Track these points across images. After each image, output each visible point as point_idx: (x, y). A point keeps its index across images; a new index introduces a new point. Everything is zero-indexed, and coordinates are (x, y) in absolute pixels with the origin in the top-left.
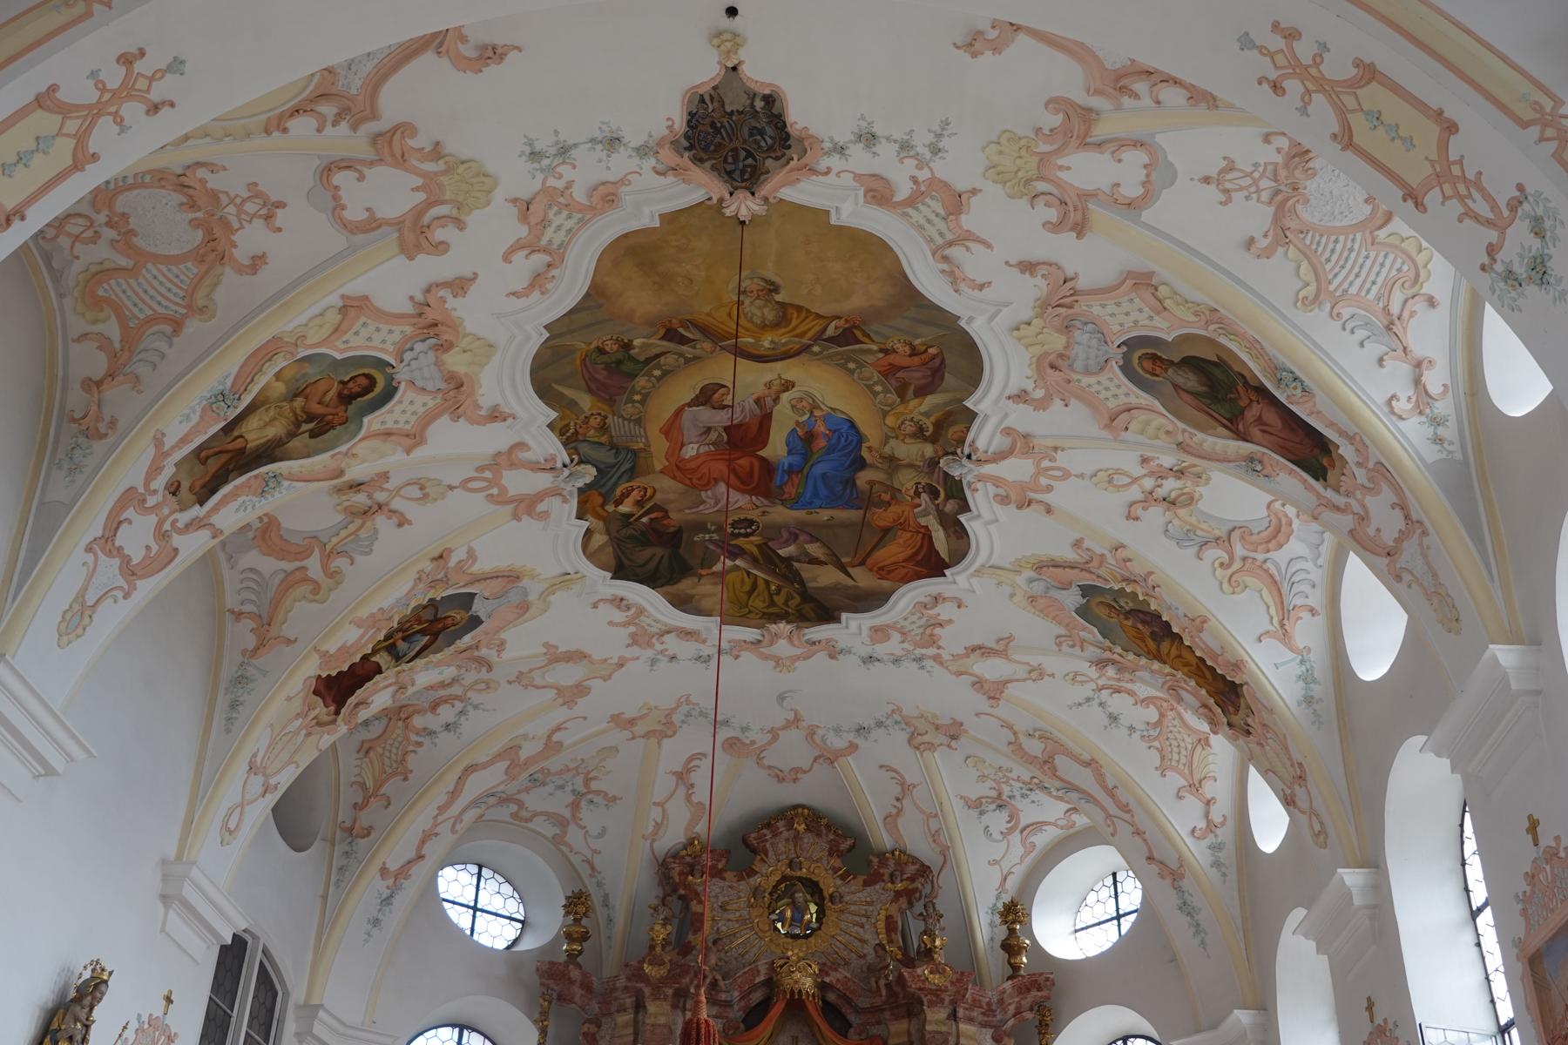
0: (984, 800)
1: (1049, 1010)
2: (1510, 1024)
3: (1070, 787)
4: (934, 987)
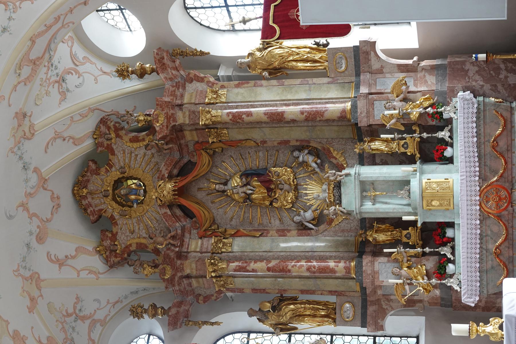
0: (61, 90)
1: (174, 51)
2: (119, 6)
3: (48, 48)
4: (166, 120)
